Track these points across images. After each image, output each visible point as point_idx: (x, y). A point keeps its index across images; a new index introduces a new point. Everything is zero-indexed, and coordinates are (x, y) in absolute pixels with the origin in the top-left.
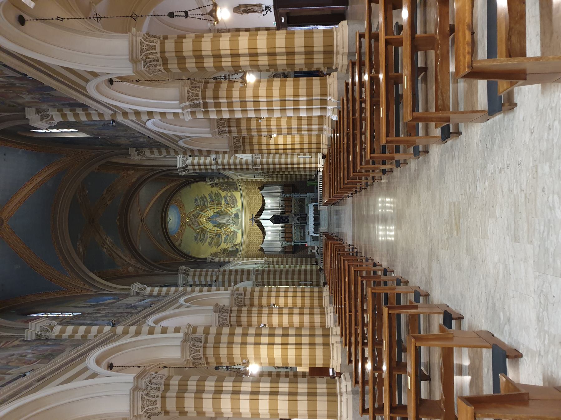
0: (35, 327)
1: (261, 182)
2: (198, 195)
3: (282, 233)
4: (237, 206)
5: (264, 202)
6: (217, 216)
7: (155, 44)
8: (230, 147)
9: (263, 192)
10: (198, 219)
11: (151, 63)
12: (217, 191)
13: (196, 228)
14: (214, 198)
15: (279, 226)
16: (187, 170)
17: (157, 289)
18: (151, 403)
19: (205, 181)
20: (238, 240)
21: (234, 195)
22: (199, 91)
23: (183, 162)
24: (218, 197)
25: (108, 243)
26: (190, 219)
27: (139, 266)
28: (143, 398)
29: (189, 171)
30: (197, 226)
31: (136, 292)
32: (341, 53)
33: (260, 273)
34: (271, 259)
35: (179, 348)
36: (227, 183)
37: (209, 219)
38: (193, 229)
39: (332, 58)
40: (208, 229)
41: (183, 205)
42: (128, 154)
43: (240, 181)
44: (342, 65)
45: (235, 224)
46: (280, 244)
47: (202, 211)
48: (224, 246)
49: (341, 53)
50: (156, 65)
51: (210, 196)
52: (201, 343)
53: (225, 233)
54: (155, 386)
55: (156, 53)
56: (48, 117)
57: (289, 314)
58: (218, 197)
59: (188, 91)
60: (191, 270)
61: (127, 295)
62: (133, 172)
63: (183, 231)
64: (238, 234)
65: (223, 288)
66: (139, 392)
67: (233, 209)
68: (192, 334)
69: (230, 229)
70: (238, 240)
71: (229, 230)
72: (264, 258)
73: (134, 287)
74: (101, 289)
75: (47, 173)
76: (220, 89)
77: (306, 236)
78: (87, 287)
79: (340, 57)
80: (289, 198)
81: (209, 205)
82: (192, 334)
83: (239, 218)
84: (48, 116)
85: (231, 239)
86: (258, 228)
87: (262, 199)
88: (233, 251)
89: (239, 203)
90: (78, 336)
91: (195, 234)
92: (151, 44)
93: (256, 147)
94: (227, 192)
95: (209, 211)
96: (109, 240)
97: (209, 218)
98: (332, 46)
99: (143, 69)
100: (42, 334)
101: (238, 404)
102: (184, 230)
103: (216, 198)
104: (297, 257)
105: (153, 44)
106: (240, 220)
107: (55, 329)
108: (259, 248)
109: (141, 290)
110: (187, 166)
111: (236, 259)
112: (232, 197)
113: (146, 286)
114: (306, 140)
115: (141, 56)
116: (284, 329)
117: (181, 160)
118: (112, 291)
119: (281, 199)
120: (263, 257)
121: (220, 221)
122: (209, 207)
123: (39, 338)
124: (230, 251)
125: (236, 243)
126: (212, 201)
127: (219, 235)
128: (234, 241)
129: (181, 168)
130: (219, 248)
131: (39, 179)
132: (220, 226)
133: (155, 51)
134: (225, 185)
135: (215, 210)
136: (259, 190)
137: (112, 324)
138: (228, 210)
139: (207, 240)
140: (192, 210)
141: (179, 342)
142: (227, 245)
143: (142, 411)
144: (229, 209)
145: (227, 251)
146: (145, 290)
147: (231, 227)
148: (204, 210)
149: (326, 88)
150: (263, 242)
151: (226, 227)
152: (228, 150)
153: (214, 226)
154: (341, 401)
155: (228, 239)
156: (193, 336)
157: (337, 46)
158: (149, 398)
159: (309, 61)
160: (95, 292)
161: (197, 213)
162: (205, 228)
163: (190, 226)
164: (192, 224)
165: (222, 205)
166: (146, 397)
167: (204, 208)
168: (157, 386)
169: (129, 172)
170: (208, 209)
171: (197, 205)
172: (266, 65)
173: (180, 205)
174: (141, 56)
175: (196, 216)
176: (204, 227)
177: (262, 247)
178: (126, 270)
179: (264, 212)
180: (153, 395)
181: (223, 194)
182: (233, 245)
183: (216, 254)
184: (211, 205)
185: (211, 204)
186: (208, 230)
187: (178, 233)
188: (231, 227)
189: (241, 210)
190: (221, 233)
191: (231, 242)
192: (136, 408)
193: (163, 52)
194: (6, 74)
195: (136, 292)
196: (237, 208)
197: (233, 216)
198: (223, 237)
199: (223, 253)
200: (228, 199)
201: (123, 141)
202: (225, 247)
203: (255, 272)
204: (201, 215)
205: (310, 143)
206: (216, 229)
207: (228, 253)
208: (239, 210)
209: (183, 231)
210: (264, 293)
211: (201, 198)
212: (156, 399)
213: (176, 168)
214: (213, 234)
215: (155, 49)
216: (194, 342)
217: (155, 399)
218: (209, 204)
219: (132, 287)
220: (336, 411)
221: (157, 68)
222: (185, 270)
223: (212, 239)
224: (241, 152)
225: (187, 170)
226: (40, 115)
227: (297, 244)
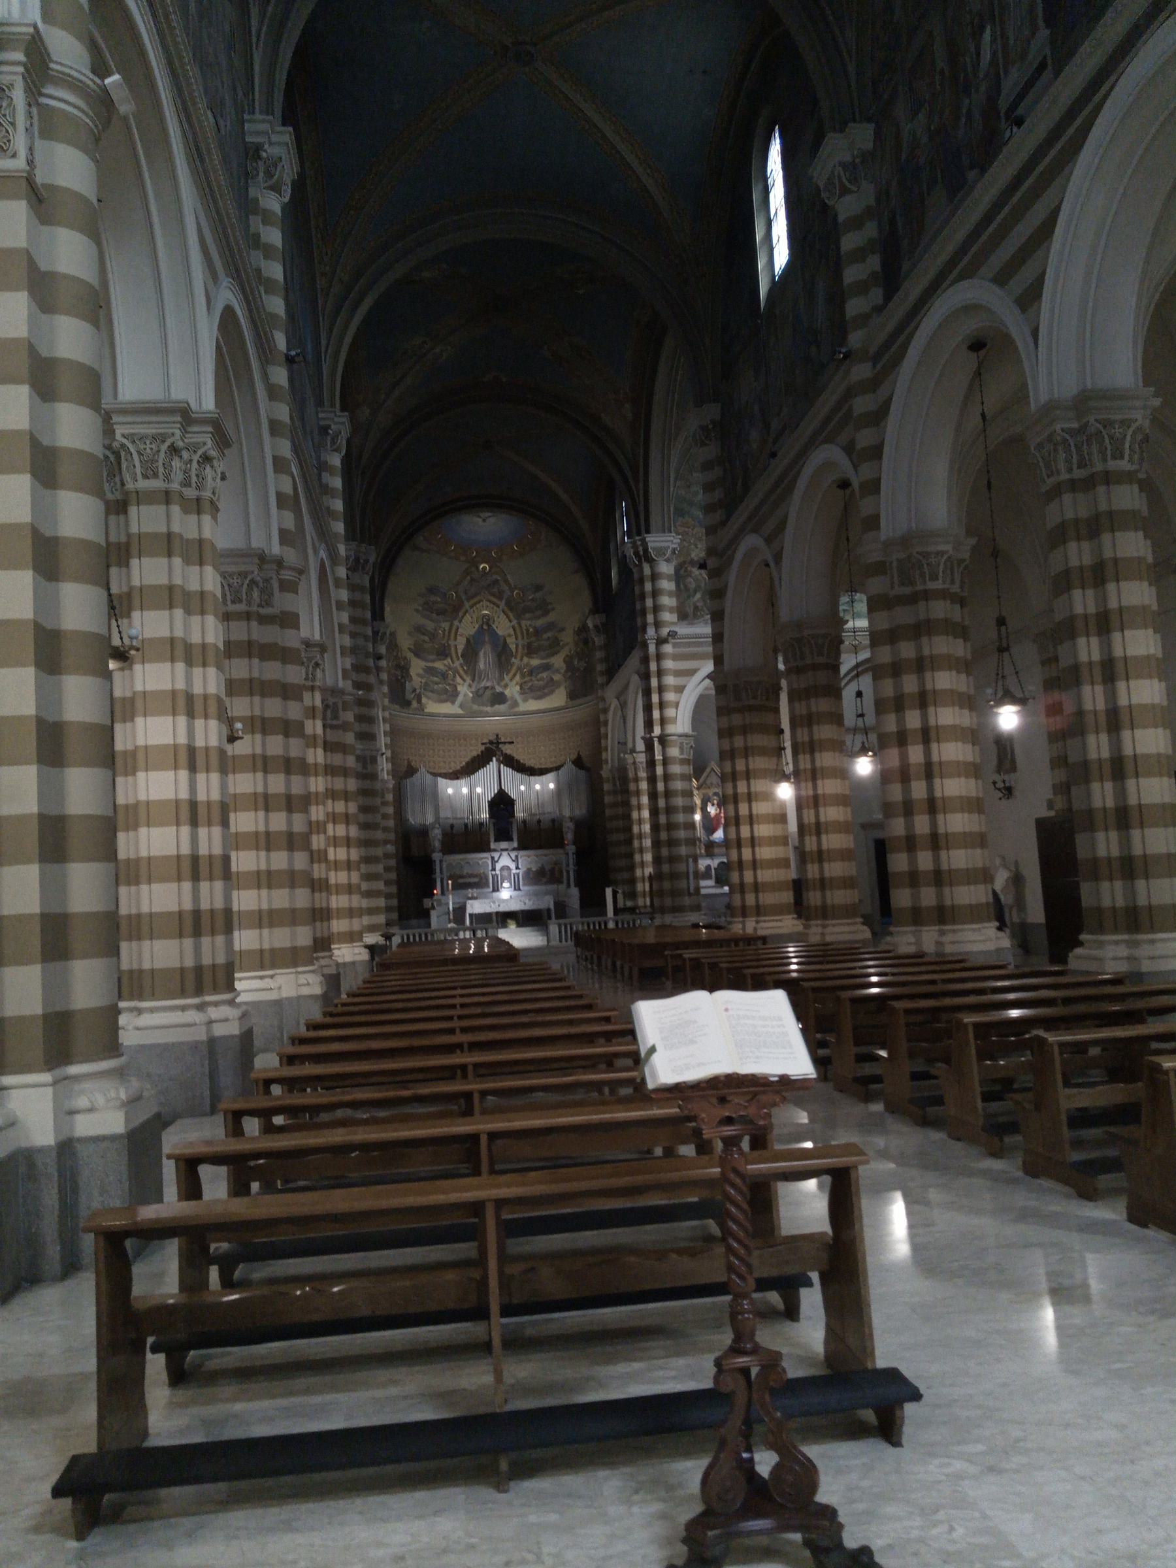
4: (525, 700)
5: (542, 772)
7: (1127, 457)
9: (569, 767)
12: (564, 645)
14: (545, 636)
16: (640, 561)
17: (337, 483)
18: (147, 462)
19: (595, 610)
20: (433, 707)
22: (944, 583)
23: (661, 552)
25: (437, 350)
28: (162, 438)
30: (466, 592)
32: (1137, 953)
33: (367, 769)
34: (390, 797)
37: (486, 626)
38: (458, 584)
39: (1116, 930)
43: (601, 706)
44: (1100, 959)
45: (478, 695)
46: (430, 820)
47: (508, 604)
48: (417, 667)
49: (1137, 953)
50: (1068, 461)
51: (551, 626)
52: (258, 606)
53: (450, 668)
54: (193, 473)
55: (1105, 460)
56: (850, 182)
57: (195, 859)
59: (942, 553)
61: (319, 403)
63: (453, 554)
64: (449, 704)
65: (348, 666)
66: (179, 425)
67: (518, 688)
68: (279, 579)
69: (461, 682)
70: (433, 707)
71: (458, 680)
72: (391, 777)
74: (331, 332)
76: (951, 638)
77: (464, 892)
79: (1123, 951)
80: (562, 838)
81: (524, 623)
82: (279, 579)
83: (492, 705)
86: (468, 759)
87: (549, 765)
89: (533, 705)
92: (1127, 445)
93: (739, 742)
94: (563, 671)
95: (508, 624)
97: (489, 626)
98: (1152, 929)
99: (1058, 427)
100: (260, 162)
101: (160, 713)
105: (1127, 452)
106: (489, 709)
107: (273, 195)
108: (413, 763)
109: (333, 439)
110: (651, 561)
111: (386, 701)
114: (765, 875)
115: (1096, 420)
117: (666, 544)
118: (328, 357)
121: (481, 654)
122: (519, 624)
125: (424, 700)
126: (537, 632)
127: (443, 653)
128: (430, 694)
129: (644, 541)
130: (410, 655)
132: (470, 654)
133: (1109, 457)
134: (583, 664)
136: (574, 757)
137: (293, 353)
138: (515, 675)
139: (431, 620)
140: (509, 577)
141: (257, 543)
143: (123, 436)
144: (518, 678)
145: (402, 677)
147: (466, 684)
148: (511, 609)
149: (972, 922)
150: (431, 773)
151: (466, 672)
152: (726, 667)
153: (468, 640)
155: (435, 679)
157: (1153, 942)
158: (162, 455)
162: (461, 614)
164: (472, 580)
165: (525, 660)
166: (164, 447)
167: (516, 609)
168: (194, 479)
169: (627, 406)
170: (515, 622)
174: (1096, 420)
176: (463, 610)
177: (419, 773)
179: (515, 773)
180: (172, 467)
181: (558, 661)
182: (418, 691)
183: (393, 646)
184: (524, 627)
185: (528, 630)
186: (456, 623)
188: (466, 684)
189: (516, 709)
190: (449, 660)
191: (426, 687)
194: (1006, 72)
195: (329, 427)
196: (520, 701)
197: (498, 689)
198: (439, 665)
199: (398, 666)
200: (545, 675)
202: (413, 672)
204: (499, 603)
205: (757, 887)
206: (461, 644)
207: (397, 680)
210: (342, 779)
214: (446, 638)
215: (1114, 458)
216: (261, 585)
217: (160, 475)
218: (529, 622)
219: (338, 413)
220: (153, 994)
221: (1062, 466)
222: (367, 561)
223: (433, 636)
225: (640, 561)
227: (438, 870)
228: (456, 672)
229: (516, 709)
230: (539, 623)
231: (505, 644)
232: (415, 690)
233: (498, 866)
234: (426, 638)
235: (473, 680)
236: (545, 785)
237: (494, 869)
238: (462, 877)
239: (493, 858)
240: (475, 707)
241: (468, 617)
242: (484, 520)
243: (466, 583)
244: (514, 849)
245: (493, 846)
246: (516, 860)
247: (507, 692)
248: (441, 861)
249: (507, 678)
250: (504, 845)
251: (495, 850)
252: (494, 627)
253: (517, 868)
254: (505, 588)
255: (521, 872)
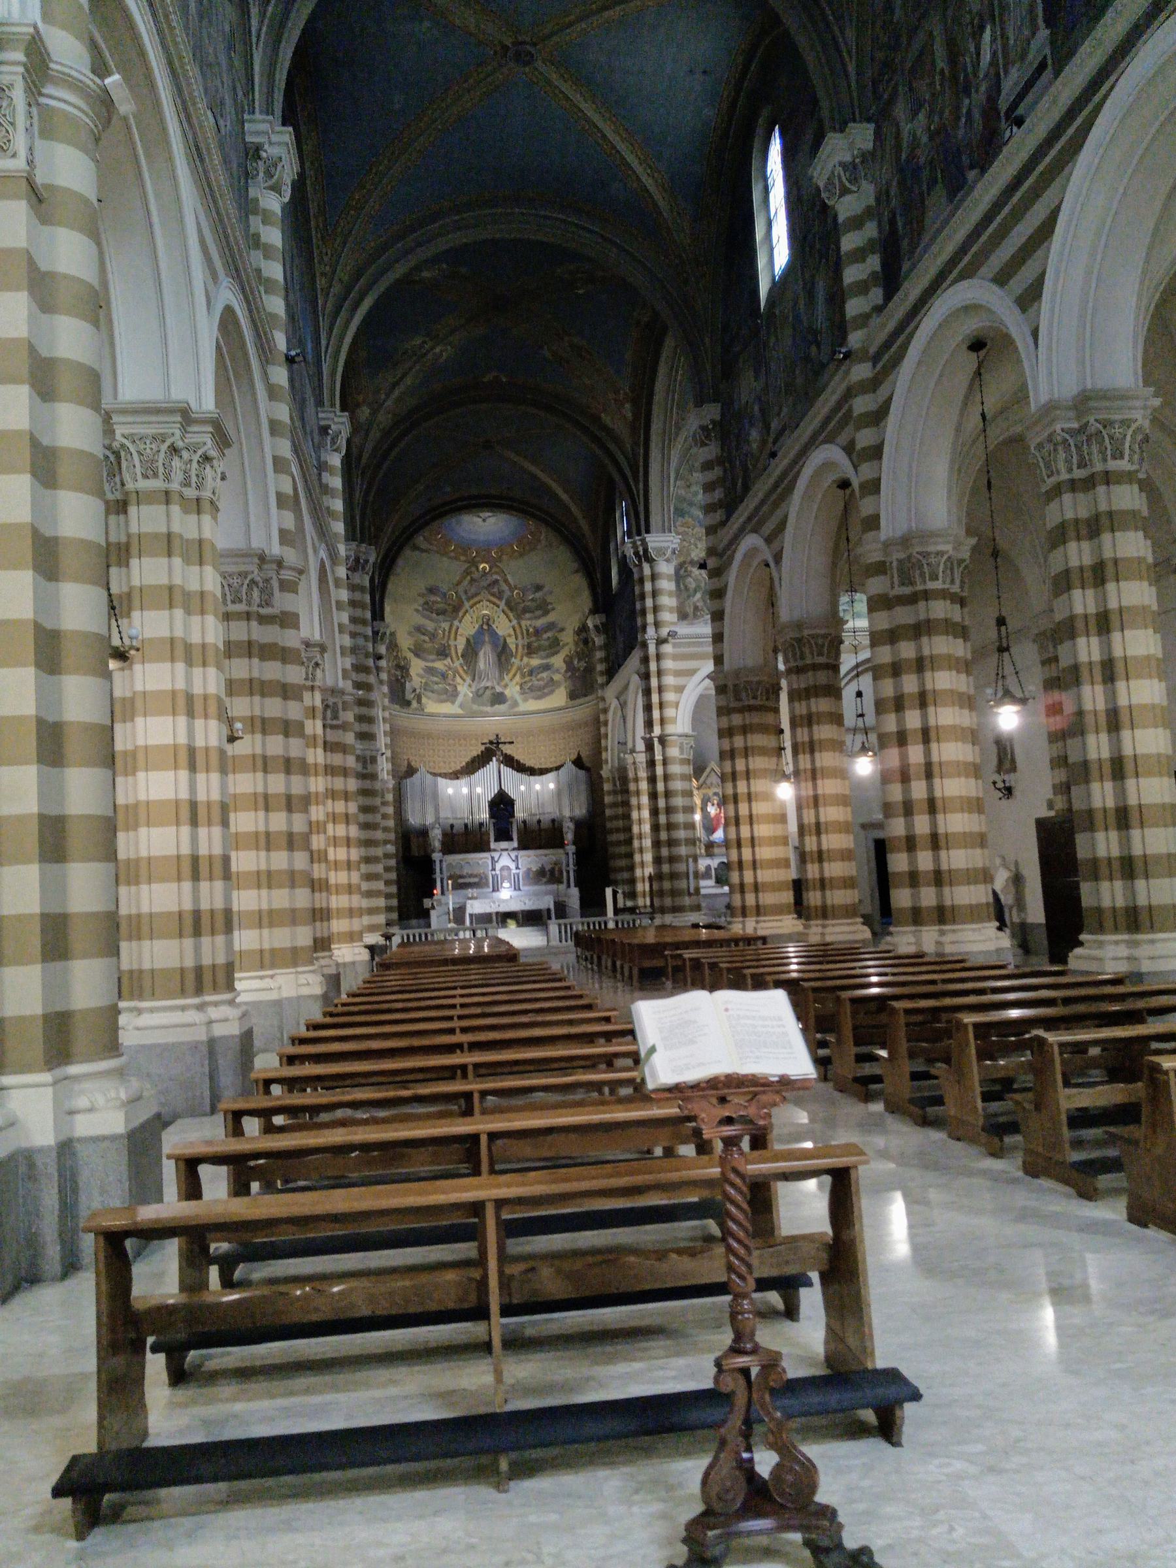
0: (279, 144)
1: (598, 762)
2: (551, 593)
3: (539, 822)
4: (525, 700)
5: (542, 772)
6: (495, 645)
7: (1127, 457)
8: (737, 673)
9: (569, 767)
10: (484, 594)
11: (1073, 449)
12: (564, 645)
13: (461, 589)
14: (545, 636)
15: (484, 815)
16: (640, 561)
19: (594, 611)
20: (432, 706)
21: (557, 691)
22: (944, 582)
23: (661, 552)
24: (550, 647)
25: (437, 350)
26: (485, 574)
27: (371, 435)
29: (636, 565)
30: (466, 592)
31: (329, 427)
32: (1137, 952)
35: (242, 545)
36: (589, 670)
37: (486, 627)
38: (459, 583)
40: (460, 622)
41: (521, 555)
42: (700, 402)
43: (601, 706)
45: (478, 695)
47: (508, 604)
48: (417, 667)
49: (1137, 952)
50: (1068, 461)
51: (551, 626)
53: (450, 669)
55: (1105, 460)
58: (550, 647)
60: (367, 579)
61: (319, 403)
62: (629, 415)
63: (452, 554)
64: (449, 704)
65: (348, 666)
67: (518, 688)
70: (432, 706)
71: (458, 679)
73: (341, 420)
75: (649, 182)
78: (336, 289)
79: (1123, 951)
80: (562, 838)
81: (523, 623)
84: (854, 180)
85: (436, 687)
87: (549, 766)
88: (403, 692)
89: (533, 705)
90: (256, 258)
91: (444, 588)
93: (739, 741)
96: (443, 352)
97: (488, 624)
102: (456, 558)
103: (547, 643)
104: (398, 870)
106: (488, 709)
110: (650, 561)
111: (386, 701)
112: (551, 684)
113: (344, 452)
115: (1096, 420)
116: (306, 837)
117: (666, 545)
119: (469, 822)
120: (394, 777)
121: (481, 654)
122: (519, 624)
123: (254, 152)
124: (403, 686)
125: (424, 700)
126: (537, 632)
127: (443, 653)
128: (430, 694)
129: (644, 541)
130: (410, 655)
131: (631, 159)
132: (470, 653)
133: (1109, 457)
134: (583, 664)
135: (511, 642)
136: (574, 757)
137: (293, 353)
138: (515, 675)
140: (509, 577)
141: (257, 543)
142: (418, 675)
144: (518, 678)
146: (335, 450)
147: (466, 684)
148: (511, 609)
149: (972, 921)
151: (466, 672)
153: (468, 640)
154: (183, 1008)
156: (275, 584)
157: (1152, 942)
159: (1104, 870)
160: (324, 308)
161: (501, 592)
162: (461, 614)
163: (467, 572)
164: (472, 580)
165: (525, 659)
166: (164, 447)
167: (516, 609)
168: (194, 479)
169: (628, 406)
170: (515, 622)
171: (524, 590)
172: (1085, 755)
173: (526, 547)
175: (493, 589)
178: (360, 398)
179: (515, 773)
181: (558, 661)
183: (393, 646)
185: (528, 631)
186: (456, 623)
187: (447, 543)
188: (466, 684)
189: (516, 709)
191: (426, 687)
192: (130, 419)
193: (1108, 478)
195: (329, 427)
197: (498, 689)
198: (439, 665)
199: (398, 667)
200: (544, 675)
201: (748, 387)
202: (413, 672)
203: (368, 753)
206: (461, 644)
207: (397, 680)
208: (515, 704)
209: (452, 554)
210: (342, 779)
211: (544, 600)
212: (161, 477)
213: (643, 530)
215: (1114, 458)
216: (261, 585)
217: (160, 474)
218: (529, 622)
219: (338, 413)
221: (1062, 466)
222: (367, 561)
223: (433, 636)
224: (723, 703)
225: (640, 561)
226: (857, 160)
228: (456, 672)
229: (516, 709)
230: (540, 623)
231: (505, 644)
232: (414, 690)
233: (498, 866)
234: (427, 638)
235: (473, 680)
236: (545, 786)
237: (494, 869)
238: (461, 877)
239: (493, 858)
240: (475, 707)
241: (468, 617)
242: (484, 520)
243: (466, 582)
244: (514, 849)
245: (493, 845)
246: (516, 860)
247: (507, 692)
248: (441, 861)
249: (507, 678)
250: (504, 845)
251: (495, 850)
252: (494, 626)
253: (517, 868)
254: (505, 587)
255: (521, 872)
